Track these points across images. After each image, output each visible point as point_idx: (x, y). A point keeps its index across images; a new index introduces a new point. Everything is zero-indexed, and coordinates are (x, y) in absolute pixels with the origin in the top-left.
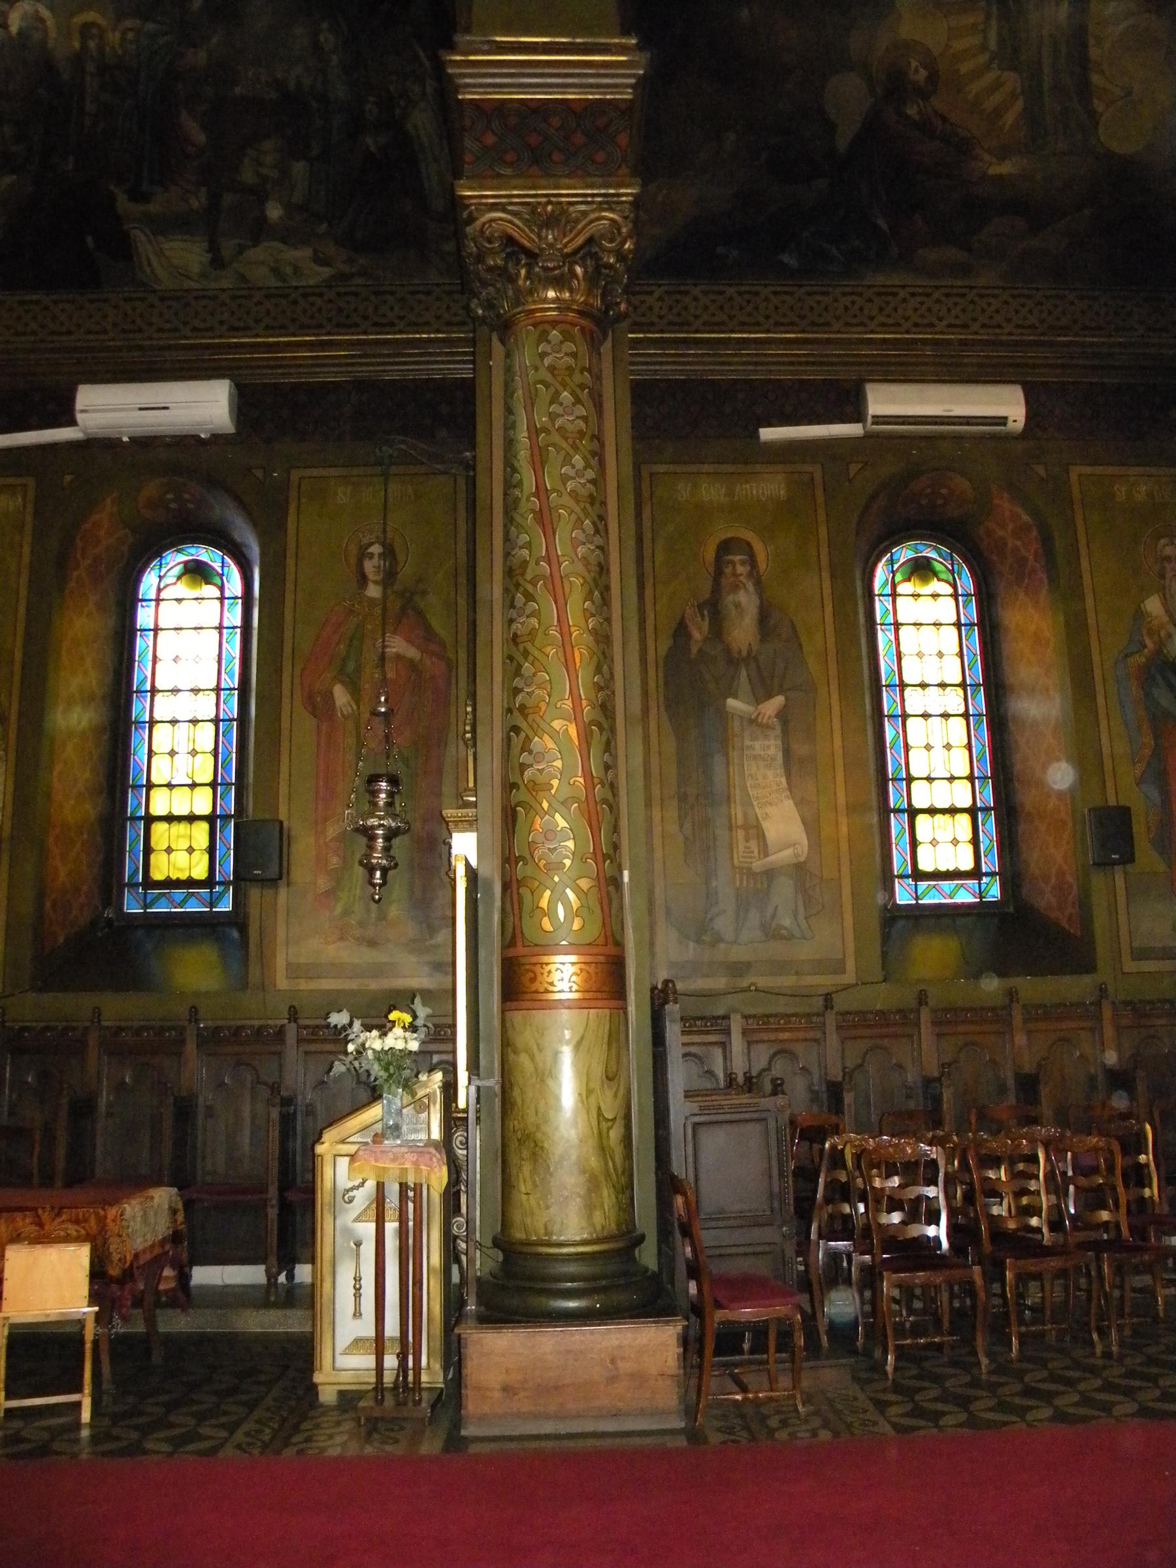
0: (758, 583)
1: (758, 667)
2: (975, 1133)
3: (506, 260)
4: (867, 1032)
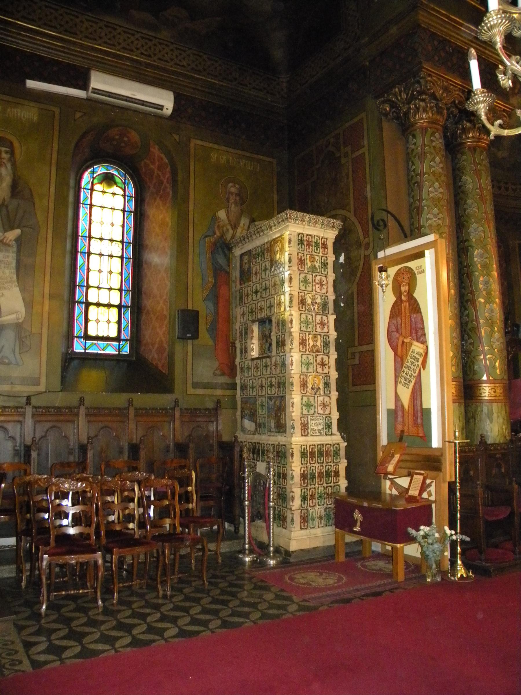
0: (14, 165)
1: (8, 211)
2: (102, 476)
4: (50, 418)
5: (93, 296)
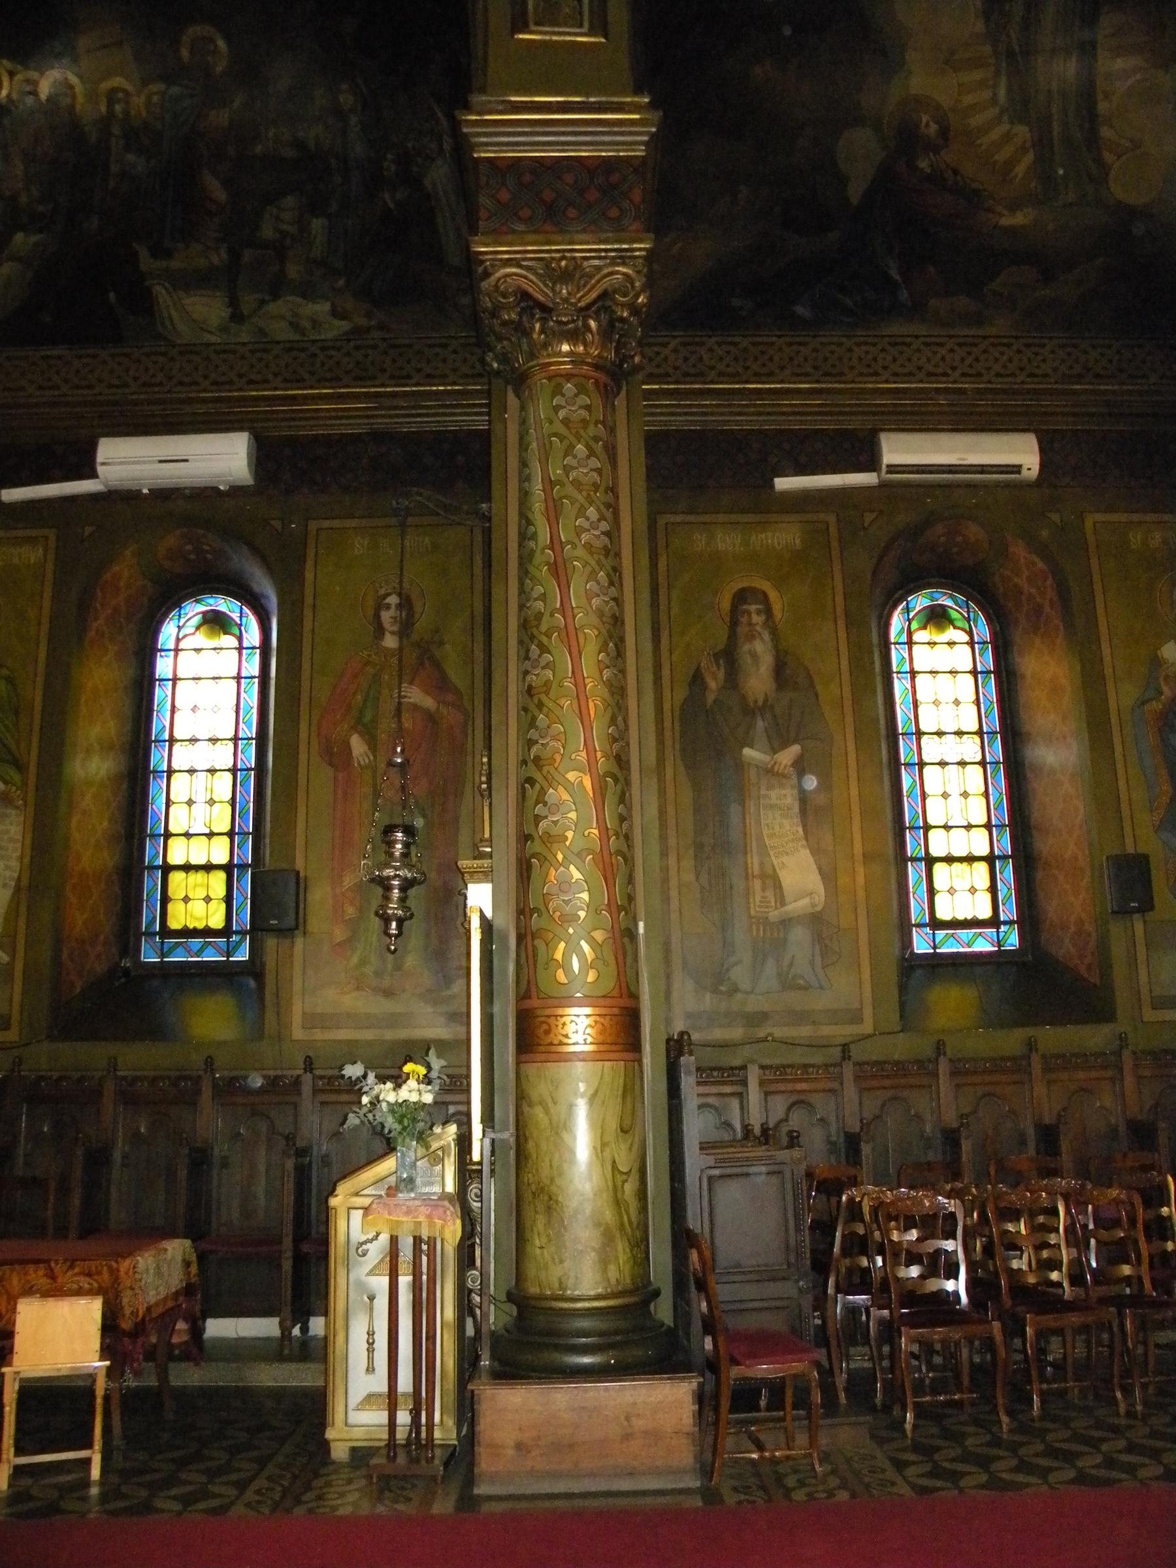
0: (774, 632)
1: (775, 717)
3: (520, 315)
5: (939, 844)
